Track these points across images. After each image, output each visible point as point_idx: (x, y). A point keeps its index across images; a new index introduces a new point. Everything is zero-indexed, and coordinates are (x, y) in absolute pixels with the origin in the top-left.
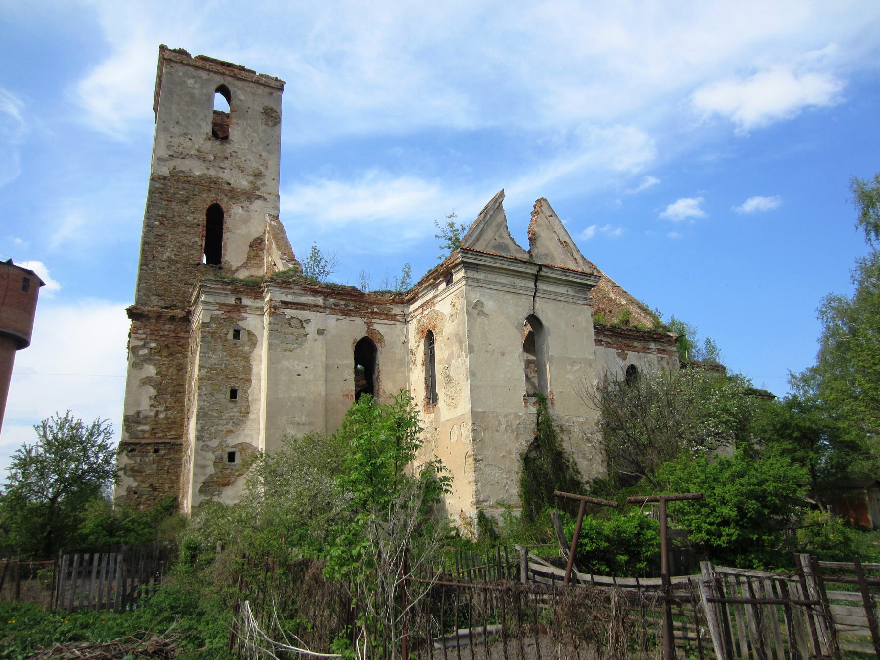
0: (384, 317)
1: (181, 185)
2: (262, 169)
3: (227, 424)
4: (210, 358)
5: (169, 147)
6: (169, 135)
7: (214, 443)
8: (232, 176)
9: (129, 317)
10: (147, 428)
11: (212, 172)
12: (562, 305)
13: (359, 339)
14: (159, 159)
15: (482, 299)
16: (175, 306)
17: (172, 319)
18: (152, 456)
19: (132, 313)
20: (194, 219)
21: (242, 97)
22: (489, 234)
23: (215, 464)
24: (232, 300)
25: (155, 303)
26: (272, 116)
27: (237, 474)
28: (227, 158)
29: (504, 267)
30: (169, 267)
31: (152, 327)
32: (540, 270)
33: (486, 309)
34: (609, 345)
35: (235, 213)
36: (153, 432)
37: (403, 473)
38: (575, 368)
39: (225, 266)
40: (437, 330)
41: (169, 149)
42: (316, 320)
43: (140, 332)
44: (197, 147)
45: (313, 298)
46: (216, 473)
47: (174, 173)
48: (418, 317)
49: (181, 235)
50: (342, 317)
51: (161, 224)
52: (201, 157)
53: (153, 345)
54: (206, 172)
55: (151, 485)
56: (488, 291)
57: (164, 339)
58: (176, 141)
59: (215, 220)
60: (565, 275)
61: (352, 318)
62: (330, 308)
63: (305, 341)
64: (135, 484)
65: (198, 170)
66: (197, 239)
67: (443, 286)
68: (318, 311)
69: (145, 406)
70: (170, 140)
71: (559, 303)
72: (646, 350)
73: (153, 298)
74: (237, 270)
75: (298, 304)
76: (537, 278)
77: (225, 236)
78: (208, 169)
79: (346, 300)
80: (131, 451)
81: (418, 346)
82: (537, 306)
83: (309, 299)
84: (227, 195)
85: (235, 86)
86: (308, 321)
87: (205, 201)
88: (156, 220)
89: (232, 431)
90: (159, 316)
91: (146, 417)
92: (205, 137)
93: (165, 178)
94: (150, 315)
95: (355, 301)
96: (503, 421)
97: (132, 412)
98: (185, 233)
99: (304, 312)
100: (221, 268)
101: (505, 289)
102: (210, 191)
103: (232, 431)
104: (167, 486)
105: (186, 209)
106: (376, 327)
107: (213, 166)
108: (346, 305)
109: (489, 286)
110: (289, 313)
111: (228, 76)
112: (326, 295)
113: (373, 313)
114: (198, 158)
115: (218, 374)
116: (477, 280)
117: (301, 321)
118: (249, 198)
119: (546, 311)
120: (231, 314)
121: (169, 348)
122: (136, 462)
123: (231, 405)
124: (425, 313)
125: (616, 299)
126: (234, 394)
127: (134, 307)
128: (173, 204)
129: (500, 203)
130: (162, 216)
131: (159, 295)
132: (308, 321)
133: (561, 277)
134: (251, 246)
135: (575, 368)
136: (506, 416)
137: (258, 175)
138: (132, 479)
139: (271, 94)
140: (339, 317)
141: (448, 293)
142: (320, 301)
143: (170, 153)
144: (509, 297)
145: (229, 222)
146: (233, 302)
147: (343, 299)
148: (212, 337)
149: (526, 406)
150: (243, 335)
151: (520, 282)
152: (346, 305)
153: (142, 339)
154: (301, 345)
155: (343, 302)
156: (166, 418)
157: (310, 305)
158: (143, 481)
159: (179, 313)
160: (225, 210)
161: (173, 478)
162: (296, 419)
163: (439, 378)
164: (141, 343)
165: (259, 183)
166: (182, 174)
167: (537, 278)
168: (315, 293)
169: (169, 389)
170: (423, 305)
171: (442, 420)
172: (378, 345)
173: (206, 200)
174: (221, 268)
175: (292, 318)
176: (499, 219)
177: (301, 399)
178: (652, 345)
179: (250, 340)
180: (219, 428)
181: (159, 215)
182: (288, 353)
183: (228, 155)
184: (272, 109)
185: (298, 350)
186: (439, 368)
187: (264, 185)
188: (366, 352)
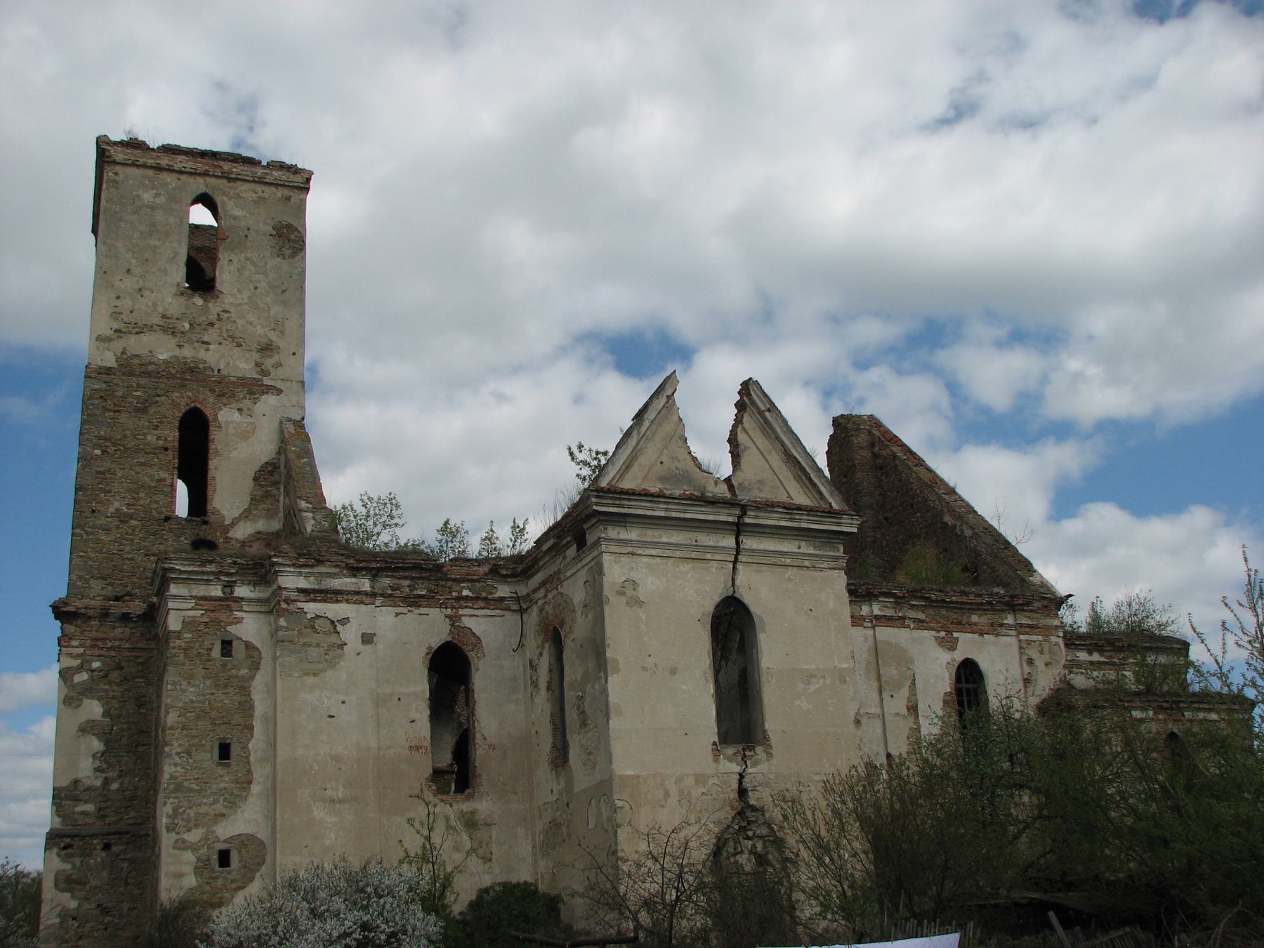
0: (481, 603)
1: (134, 381)
2: (274, 337)
3: (216, 802)
4: (184, 691)
5: (116, 315)
6: (113, 296)
7: (194, 836)
9: (56, 618)
10: (89, 807)
11: (188, 352)
12: (790, 572)
13: (435, 646)
14: (99, 339)
15: (634, 575)
17: (125, 618)
18: (100, 856)
19: (60, 611)
20: (159, 438)
21: (238, 212)
22: (649, 455)
23: (198, 871)
24: (216, 591)
26: (290, 239)
27: (234, 886)
28: (212, 324)
29: (674, 514)
30: (118, 527)
31: (94, 634)
32: (744, 513)
33: (642, 594)
34: (920, 624)
35: (227, 418)
36: (101, 814)
38: (812, 688)
39: (212, 518)
40: (566, 628)
41: (116, 319)
42: (356, 618)
43: (74, 643)
44: (160, 309)
45: (353, 580)
46: (199, 886)
48: (540, 602)
49: (138, 469)
50: (405, 610)
51: (104, 452)
52: (168, 327)
53: (96, 665)
54: (177, 352)
55: (99, 906)
56: (645, 560)
57: (113, 653)
58: (126, 304)
60: (792, 520)
62: (382, 595)
63: (340, 657)
64: (73, 904)
65: (163, 350)
66: (163, 475)
67: (572, 551)
68: (362, 602)
69: (85, 769)
70: (117, 303)
71: (781, 570)
72: (995, 629)
73: (93, 583)
74: (233, 524)
76: (738, 529)
77: (213, 463)
78: (180, 347)
79: (412, 578)
80: (65, 848)
81: (541, 654)
82: (740, 579)
83: (345, 582)
84: (213, 391)
85: (224, 194)
86: (345, 621)
87: (175, 405)
88: (95, 446)
89: (223, 815)
90: (104, 615)
91: (88, 789)
92: (174, 290)
93: (108, 371)
94: (91, 613)
95: (428, 579)
96: (673, 790)
97: (64, 782)
98: (142, 464)
100: (205, 523)
101: (678, 554)
102: (184, 386)
103: (223, 815)
104: (125, 906)
105: (144, 422)
106: (467, 622)
107: (190, 342)
108: (412, 588)
109: (648, 552)
110: (312, 608)
111: (214, 170)
112: (375, 574)
113: (460, 598)
114: (164, 329)
116: (626, 542)
117: (332, 622)
118: (251, 393)
119: (760, 590)
120: (217, 615)
121: (121, 668)
122: (74, 867)
123: (220, 770)
124: (550, 596)
125: (955, 526)
126: (225, 751)
127: (64, 602)
128: (123, 414)
129: (670, 397)
130: (106, 439)
131: (103, 578)
133: (783, 523)
134: (255, 479)
135: (812, 688)
136: (679, 780)
137: (267, 348)
138: (68, 895)
139: (288, 198)
140: (399, 610)
141: (580, 565)
142: (365, 584)
143: (116, 326)
144: (685, 567)
145: (217, 439)
147: (405, 578)
148: (186, 655)
149: (716, 760)
150: (238, 651)
151: (707, 539)
152: (412, 588)
154: (332, 664)
155: (407, 583)
156: (122, 790)
157: (348, 593)
158: (86, 899)
159: (137, 607)
160: (211, 418)
161: (137, 892)
162: (329, 792)
163: (571, 715)
164: (77, 663)
165: (269, 363)
166: (136, 361)
167: (738, 529)
168: (354, 571)
169: (124, 741)
170: (543, 584)
171: (576, 790)
172: (471, 655)
173: (179, 401)
174: (205, 523)
175: (317, 617)
176: (668, 427)
177: (337, 758)
178: (1010, 620)
179: (249, 657)
180: (203, 810)
181: (99, 438)
182: (311, 680)
183: (213, 318)
184: (289, 226)
185: (329, 673)
186: (570, 696)
187: (278, 365)
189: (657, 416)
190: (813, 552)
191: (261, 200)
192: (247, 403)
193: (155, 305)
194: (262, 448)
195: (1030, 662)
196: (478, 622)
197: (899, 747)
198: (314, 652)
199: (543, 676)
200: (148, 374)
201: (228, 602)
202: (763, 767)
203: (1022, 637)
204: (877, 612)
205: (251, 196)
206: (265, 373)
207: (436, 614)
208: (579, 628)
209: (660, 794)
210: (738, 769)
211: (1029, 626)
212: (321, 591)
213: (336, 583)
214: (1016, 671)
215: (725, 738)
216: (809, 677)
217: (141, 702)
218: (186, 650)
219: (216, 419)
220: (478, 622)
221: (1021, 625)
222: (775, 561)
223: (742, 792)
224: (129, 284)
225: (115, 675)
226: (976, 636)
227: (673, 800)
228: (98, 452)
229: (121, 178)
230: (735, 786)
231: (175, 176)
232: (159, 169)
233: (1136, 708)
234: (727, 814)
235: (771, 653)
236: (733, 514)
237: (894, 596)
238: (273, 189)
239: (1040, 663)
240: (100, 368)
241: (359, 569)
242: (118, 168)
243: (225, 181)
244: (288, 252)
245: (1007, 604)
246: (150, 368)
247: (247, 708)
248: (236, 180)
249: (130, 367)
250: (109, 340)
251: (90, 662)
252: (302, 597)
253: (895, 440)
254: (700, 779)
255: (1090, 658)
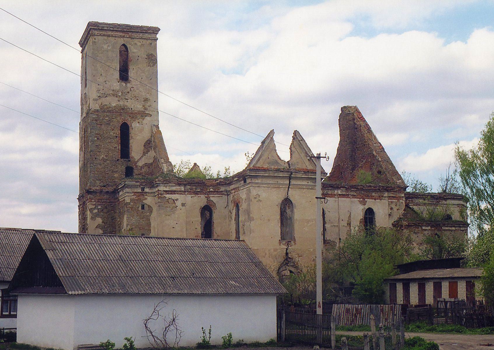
2: (148, 96)
4: (131, 220)
5: (98, 91)
8: (132, 103)
11: (121, 103)
15: (259, 193)
16: (108, 185)
17: (107, 192)
21: (135, 51)
24: (140, 190)
25: (98, 184)
28: (128, 92)
34: (354, 197)
35: (135, 126)
37: (470, 156)
39: (132, 159)
42: (180, 198)
43: (93, 201)
47: (102, 107)
51: (98, 139)
53: (99, 207)
59: (125, 131)
61: (199, 196)
65: (113, 102)
68: (181, 194)
70: (99, 87)
72: (380, 198)
73: (97, 181)
74: (138, 161)
75: (172, 191)
77: (131, 141)
82: (289, 192)
86: (177, 200)
87: (118, 122)
90: (101, 192)
94: (98, 191)
96: (267, 253)
99: (174, 195)
100: (129, 161)
106: (212, 199)
108: (196, 189)
110: (168, 196)
114: (113, 95)
115: (135, 228)
119: (295, 195)
129: (272, 138)
132: (177, 200)
136: (269, 250)
139: (151, 44)
140: (192, 196)
142: (183, 188)
145: (132, 133)
146: (140, 191)
149: (280, 245)
151: (281, 181)
153: (94, 205)
159: (110, 189)
164: (94, 207)
166: (105, 107)
167: (290, 178)
168: (179, 185)
174: (129, 161)
178: (386, 194)
183: (129, 90)
184: (151, 54)
188: (207, 211)
189: (268, 143)
190: (312, 184)
191: (143, 45)
192: (140, 120)
193: (110, 87)
194: (146, 135)
195: (391, 209)
196: (214, 198)
197: (344, 237)
198: (169, 209)
199: (234, 217)
200: (110, 111)
201: (143, 193)
202: (293, 247)
203: (390, 200)
204: (340, 193)
205: (139, 44)
206: (146, 109)
207: (203, 196)
208: (243, 206)
209: (264, 255)
210: (286, 247)
211: (392, 197)
212: (170, 191)
213: (174, 188)
214: (387, 211)
215: (283, 238)
216: (308, 221)
217: (113, 218)
218: (132, 208)
219: (131, 126)
220: (214, 198)
221: (390, 197)
222: (300, 187)
223: (287, 254)
224: (101, 80)
225: (105, 210)
226: (373, 200)
227: (267, 256)
228: (96, 139)
229: (96, 41)
230: (285, 252)
231: (114, 38)
232: (109, 36)
233: (424, 226)
234: (281, 260)
235: (298, 215)
236: (289, 173)
237: (345, 188)
238: (229, 292)
239: (395, 209)
240: (95, 110)
241: (181, 184)
242: (96, 37)
243: (130, 39)
244: (152, 65)
245: (385, 189)
246: (110, 109)
247: (149, 225)
248: (133, 38)
249: (104, 109)
250: (96, 100)
251: (97, 206)
252: (165, 193)
253: (362, 119)
254: (275, 250)
255: (424, 202)
